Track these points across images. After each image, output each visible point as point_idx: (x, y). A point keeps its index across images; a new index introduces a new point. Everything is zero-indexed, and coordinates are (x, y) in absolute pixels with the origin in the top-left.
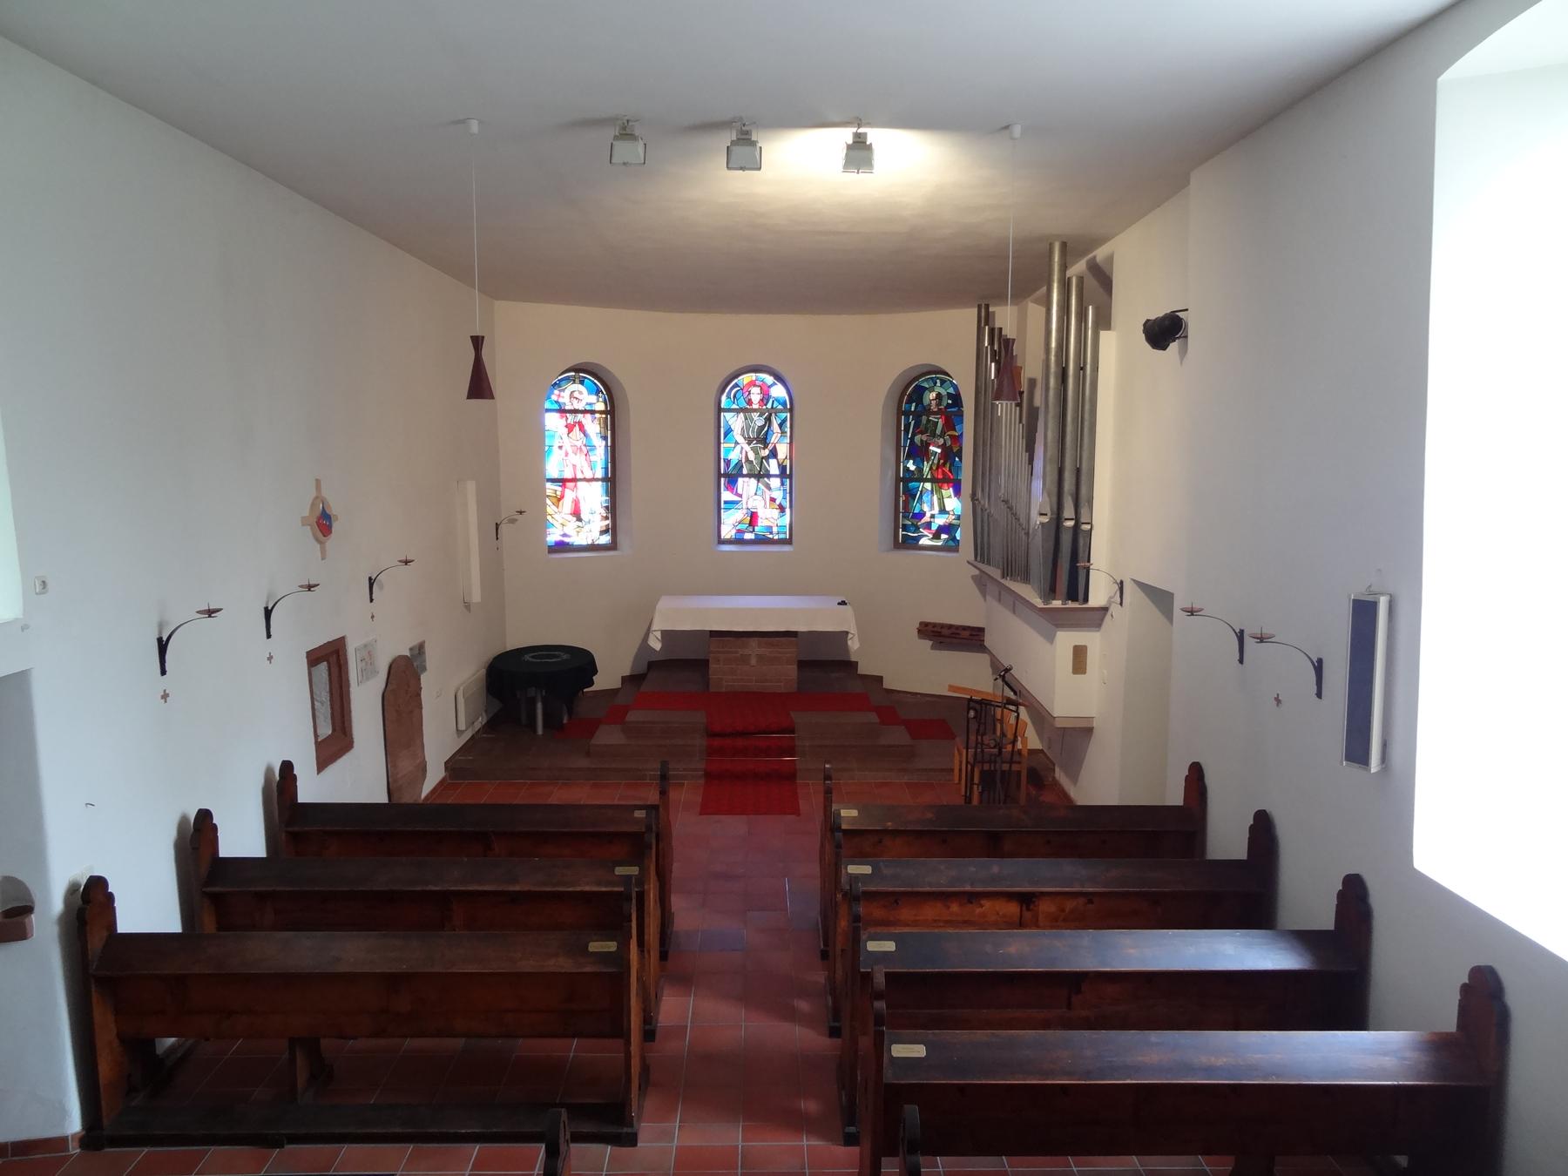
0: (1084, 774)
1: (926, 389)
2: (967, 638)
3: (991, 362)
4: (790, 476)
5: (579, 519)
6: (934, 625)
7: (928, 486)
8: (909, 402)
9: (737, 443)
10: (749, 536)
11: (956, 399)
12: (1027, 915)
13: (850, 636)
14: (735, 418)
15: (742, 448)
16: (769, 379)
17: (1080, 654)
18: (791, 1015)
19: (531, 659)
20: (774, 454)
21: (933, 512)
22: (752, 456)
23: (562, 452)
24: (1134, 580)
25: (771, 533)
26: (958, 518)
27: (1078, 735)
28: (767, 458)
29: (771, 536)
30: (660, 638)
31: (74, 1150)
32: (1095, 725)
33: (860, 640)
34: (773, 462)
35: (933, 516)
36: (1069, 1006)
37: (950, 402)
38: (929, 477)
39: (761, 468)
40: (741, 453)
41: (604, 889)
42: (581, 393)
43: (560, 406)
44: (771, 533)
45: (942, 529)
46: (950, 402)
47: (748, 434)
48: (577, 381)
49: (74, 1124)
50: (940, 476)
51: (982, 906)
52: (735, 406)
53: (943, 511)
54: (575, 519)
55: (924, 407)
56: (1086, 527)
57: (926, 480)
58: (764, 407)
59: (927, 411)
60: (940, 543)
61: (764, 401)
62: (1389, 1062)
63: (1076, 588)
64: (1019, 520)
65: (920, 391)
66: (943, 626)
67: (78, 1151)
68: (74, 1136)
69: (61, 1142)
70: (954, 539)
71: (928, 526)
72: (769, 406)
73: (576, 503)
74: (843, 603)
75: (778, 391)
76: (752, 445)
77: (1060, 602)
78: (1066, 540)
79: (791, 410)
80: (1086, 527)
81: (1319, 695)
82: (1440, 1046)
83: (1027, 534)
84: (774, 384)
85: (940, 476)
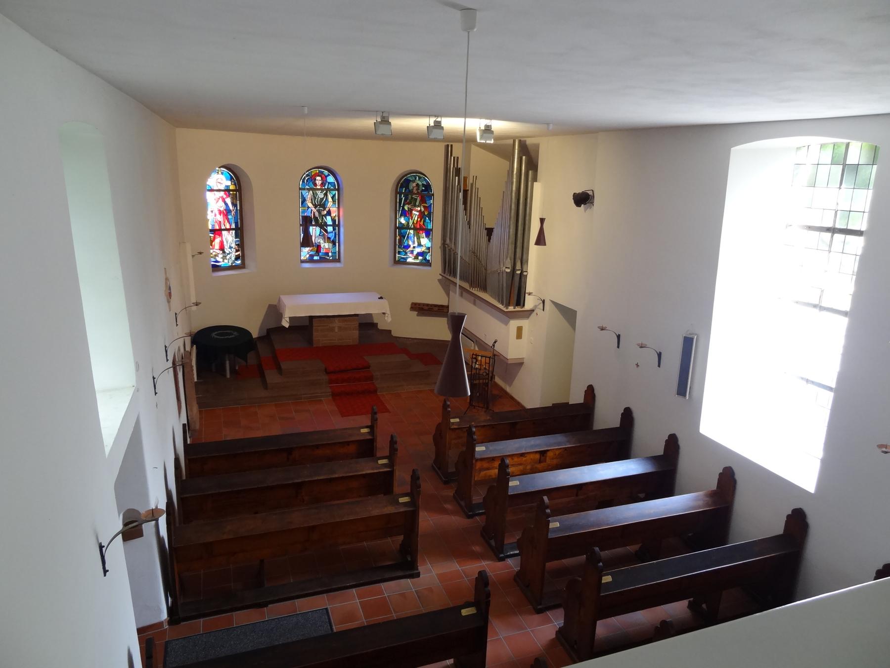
0: (516, 382)
1: (412, 181)
2: (438, 310)
3: (456, 176)
4: (339, 225)
5: (224, 252)
6: (419, 304)
7: (412, 232)
8: (402, 187)
9: (309, 207)
10: (316, 258)
11: (428, 187)
12: (543, 458)
13: (387, 315)
14: (308, 194)
15: (312, 210)
16: (326, 172)
17: (520, 330)
18: (444, 511)
19: (216, 337)
20: (329, 213)
21: (414, 245)
22: (317, 214)
23: (213, 214)
24: (551, 301)
25: (328, 256)
26: (428, 248)
27: (514, 367)
28: (325, 215)
29: (328, 258)
30: (288, 321)
31: (166, 626)
32: (525, 361)
33: (392, 317)
34: (329, 218)
35: (414, 247)
36: (577, 495)
37: (424, 188)
38: (412, 227)
39: (322, 221)
40: (311, 213)
41: (376, 471)
42: (222, 180)
43: (211, 187)
44: (328, 256)
45: (419, 254)
46: (424, 188)
47: (315, 203)
48: (220, 173)
49: (164, 616)
50: (418, 227)
51: (526, 457)
52: (307, 187)
53: (420, 245)
54: (221, 252)
55: (409, 191)
56: (525, 273)
57: (411, 229)
58: (323, 188)
59: (411, 192)
60: (418, 261)
61: (323, 184)
62: (692, 504)
63: (520, 302)
64: (481, 262)
65: (407, 182)
66: (424, 305)
67: (167, 627)
68: (165, 620)
69: (160, 624)
70: (425, 259)
71: (412, 252)
72: (326, 187)
73: (222, 244)
74: (381, 298)
75: (331, 179)
76: (317, 209)
77: (513, 307)
78: (517, 279)
79: (338, 190)
80: (525, 273)
81: (659, 366)
82: (713, 495)
83: (486, 269)
84: (329, 175)
85: (418, 227)
